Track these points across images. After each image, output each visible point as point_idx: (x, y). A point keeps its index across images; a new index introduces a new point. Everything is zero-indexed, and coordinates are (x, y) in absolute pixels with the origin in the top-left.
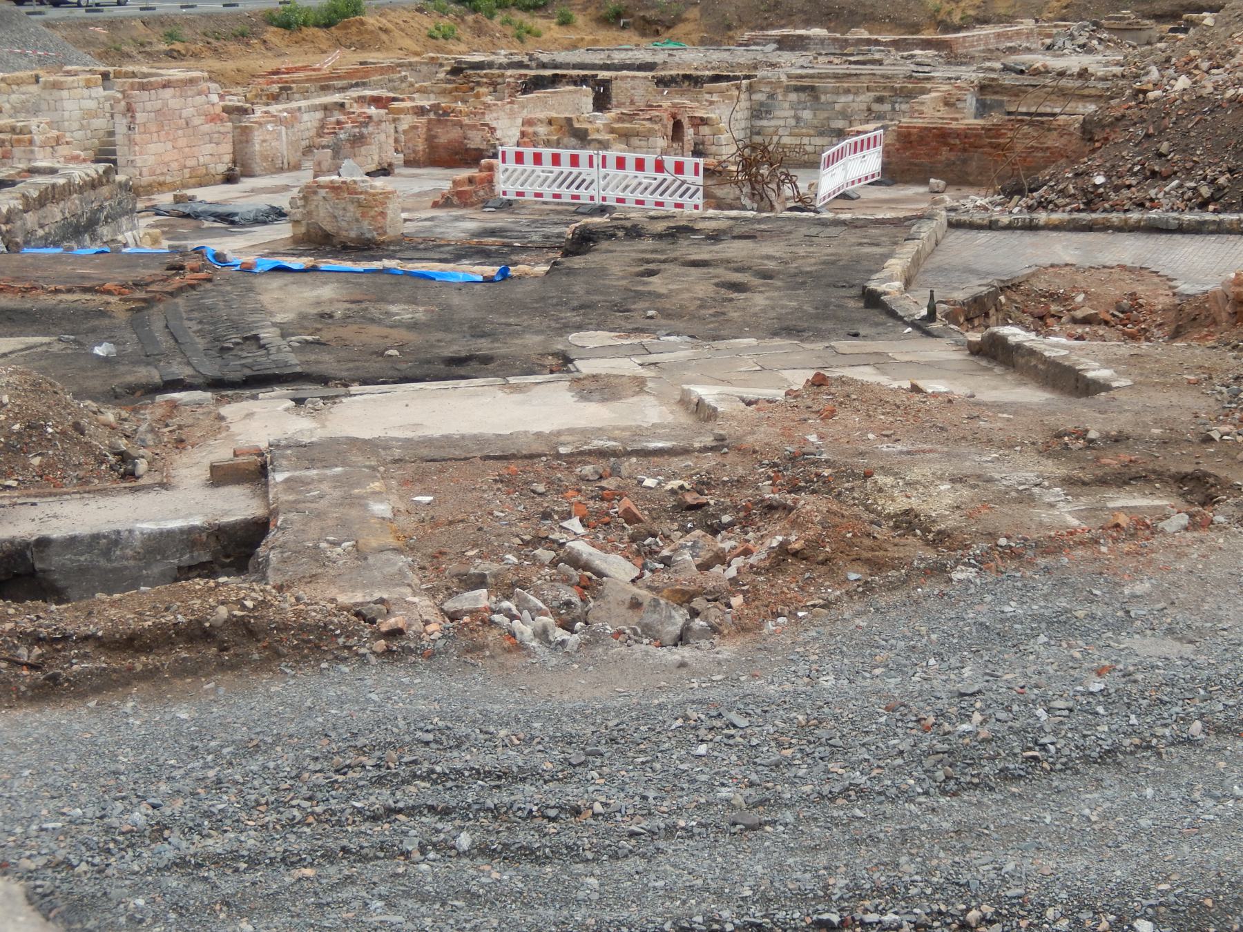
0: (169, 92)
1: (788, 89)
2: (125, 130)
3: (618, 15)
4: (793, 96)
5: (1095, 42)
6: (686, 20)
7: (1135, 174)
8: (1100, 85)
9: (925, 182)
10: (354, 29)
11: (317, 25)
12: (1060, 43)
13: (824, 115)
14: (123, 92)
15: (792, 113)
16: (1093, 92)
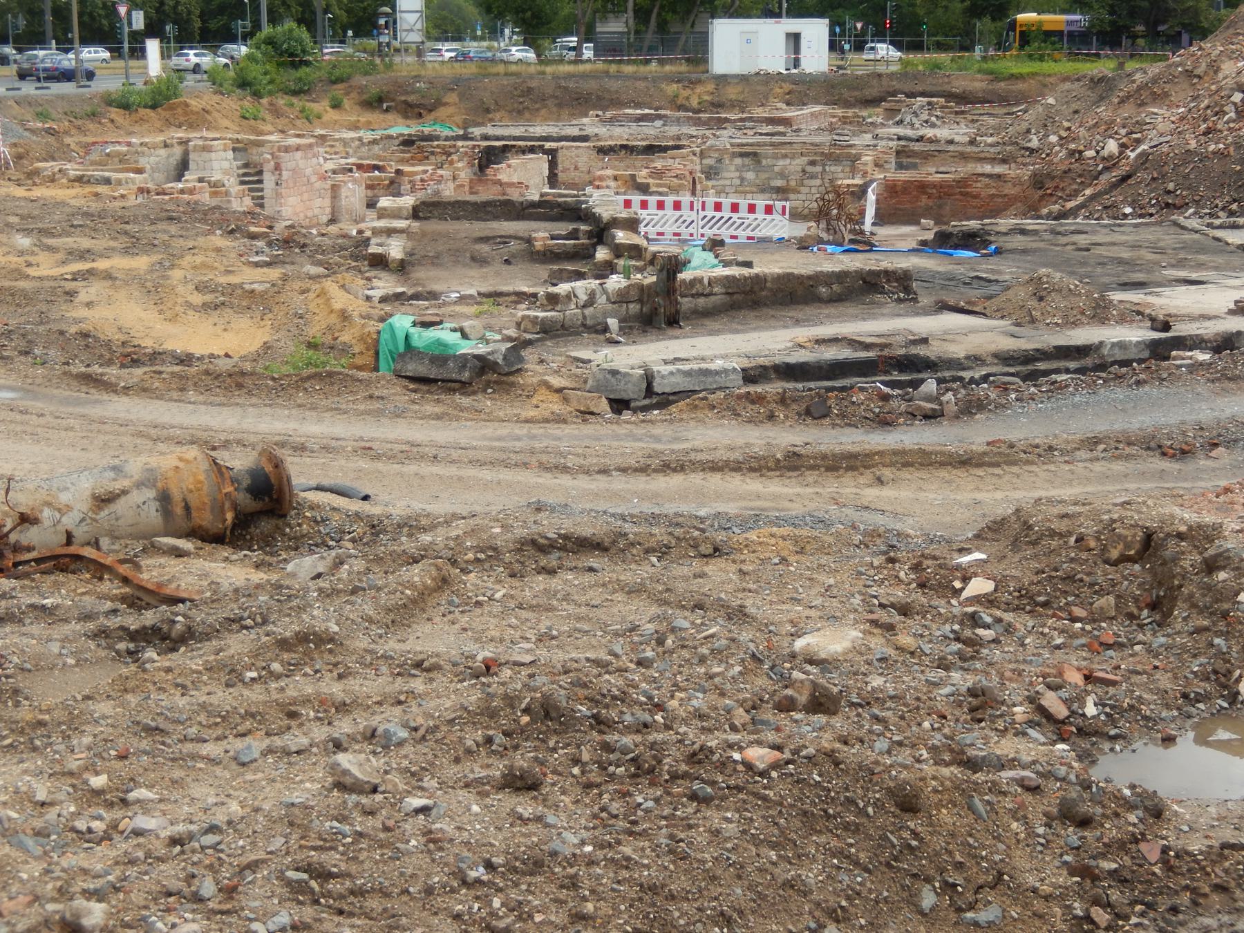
0: (299, 154)
1: (734, 155)
2: (273, 185)
3: (380, 100)
4: (738, 161)
5: (933, 119)
6: (446, 104)
7: (1153, 206)
8: (992, 150)
9: (917, 223)
10: (179, 110)
11: (145, 107)
12: (908, 120)
13: (764, 176)
14: (272, 154)
15: (737, 174)
16: (988, 155)
